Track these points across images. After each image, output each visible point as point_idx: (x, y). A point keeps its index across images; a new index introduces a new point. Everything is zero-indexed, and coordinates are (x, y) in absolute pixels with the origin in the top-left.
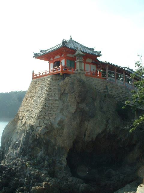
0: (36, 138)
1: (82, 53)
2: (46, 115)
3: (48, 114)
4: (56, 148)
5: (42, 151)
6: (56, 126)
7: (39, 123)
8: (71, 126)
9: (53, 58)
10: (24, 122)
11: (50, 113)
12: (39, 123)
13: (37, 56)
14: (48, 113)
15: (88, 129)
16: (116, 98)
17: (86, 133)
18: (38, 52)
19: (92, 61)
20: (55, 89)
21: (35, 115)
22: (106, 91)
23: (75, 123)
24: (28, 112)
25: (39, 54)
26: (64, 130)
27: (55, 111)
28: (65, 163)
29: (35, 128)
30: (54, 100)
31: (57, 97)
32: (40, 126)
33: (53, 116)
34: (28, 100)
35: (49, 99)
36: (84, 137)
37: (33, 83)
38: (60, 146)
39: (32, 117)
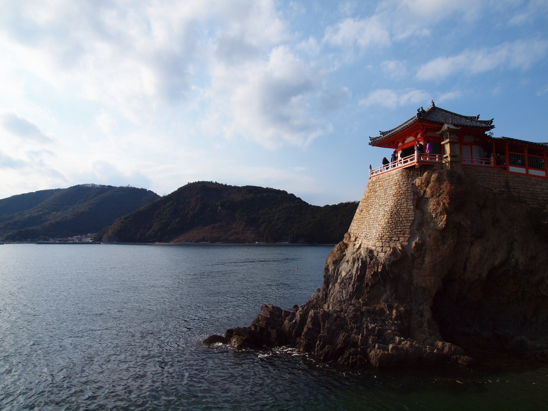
5: (388, 292)
7: (382, 247)
9: (403, 142)
10: (357, 246)
13: (376, 142)
16: (528, 203)
18: (376, 134)
20: (407, 192)
21: (375, 234)
24: (364, 230)
25: (378, 138)
26: (425, 259)
27: (408, 227)
28: (428, 315)
31: (411, 204)
33: (406, 235)
34: (363, 212)
35: (398, 208)
37: (371, 185)
38: (419, 286)
39: (371, 237)
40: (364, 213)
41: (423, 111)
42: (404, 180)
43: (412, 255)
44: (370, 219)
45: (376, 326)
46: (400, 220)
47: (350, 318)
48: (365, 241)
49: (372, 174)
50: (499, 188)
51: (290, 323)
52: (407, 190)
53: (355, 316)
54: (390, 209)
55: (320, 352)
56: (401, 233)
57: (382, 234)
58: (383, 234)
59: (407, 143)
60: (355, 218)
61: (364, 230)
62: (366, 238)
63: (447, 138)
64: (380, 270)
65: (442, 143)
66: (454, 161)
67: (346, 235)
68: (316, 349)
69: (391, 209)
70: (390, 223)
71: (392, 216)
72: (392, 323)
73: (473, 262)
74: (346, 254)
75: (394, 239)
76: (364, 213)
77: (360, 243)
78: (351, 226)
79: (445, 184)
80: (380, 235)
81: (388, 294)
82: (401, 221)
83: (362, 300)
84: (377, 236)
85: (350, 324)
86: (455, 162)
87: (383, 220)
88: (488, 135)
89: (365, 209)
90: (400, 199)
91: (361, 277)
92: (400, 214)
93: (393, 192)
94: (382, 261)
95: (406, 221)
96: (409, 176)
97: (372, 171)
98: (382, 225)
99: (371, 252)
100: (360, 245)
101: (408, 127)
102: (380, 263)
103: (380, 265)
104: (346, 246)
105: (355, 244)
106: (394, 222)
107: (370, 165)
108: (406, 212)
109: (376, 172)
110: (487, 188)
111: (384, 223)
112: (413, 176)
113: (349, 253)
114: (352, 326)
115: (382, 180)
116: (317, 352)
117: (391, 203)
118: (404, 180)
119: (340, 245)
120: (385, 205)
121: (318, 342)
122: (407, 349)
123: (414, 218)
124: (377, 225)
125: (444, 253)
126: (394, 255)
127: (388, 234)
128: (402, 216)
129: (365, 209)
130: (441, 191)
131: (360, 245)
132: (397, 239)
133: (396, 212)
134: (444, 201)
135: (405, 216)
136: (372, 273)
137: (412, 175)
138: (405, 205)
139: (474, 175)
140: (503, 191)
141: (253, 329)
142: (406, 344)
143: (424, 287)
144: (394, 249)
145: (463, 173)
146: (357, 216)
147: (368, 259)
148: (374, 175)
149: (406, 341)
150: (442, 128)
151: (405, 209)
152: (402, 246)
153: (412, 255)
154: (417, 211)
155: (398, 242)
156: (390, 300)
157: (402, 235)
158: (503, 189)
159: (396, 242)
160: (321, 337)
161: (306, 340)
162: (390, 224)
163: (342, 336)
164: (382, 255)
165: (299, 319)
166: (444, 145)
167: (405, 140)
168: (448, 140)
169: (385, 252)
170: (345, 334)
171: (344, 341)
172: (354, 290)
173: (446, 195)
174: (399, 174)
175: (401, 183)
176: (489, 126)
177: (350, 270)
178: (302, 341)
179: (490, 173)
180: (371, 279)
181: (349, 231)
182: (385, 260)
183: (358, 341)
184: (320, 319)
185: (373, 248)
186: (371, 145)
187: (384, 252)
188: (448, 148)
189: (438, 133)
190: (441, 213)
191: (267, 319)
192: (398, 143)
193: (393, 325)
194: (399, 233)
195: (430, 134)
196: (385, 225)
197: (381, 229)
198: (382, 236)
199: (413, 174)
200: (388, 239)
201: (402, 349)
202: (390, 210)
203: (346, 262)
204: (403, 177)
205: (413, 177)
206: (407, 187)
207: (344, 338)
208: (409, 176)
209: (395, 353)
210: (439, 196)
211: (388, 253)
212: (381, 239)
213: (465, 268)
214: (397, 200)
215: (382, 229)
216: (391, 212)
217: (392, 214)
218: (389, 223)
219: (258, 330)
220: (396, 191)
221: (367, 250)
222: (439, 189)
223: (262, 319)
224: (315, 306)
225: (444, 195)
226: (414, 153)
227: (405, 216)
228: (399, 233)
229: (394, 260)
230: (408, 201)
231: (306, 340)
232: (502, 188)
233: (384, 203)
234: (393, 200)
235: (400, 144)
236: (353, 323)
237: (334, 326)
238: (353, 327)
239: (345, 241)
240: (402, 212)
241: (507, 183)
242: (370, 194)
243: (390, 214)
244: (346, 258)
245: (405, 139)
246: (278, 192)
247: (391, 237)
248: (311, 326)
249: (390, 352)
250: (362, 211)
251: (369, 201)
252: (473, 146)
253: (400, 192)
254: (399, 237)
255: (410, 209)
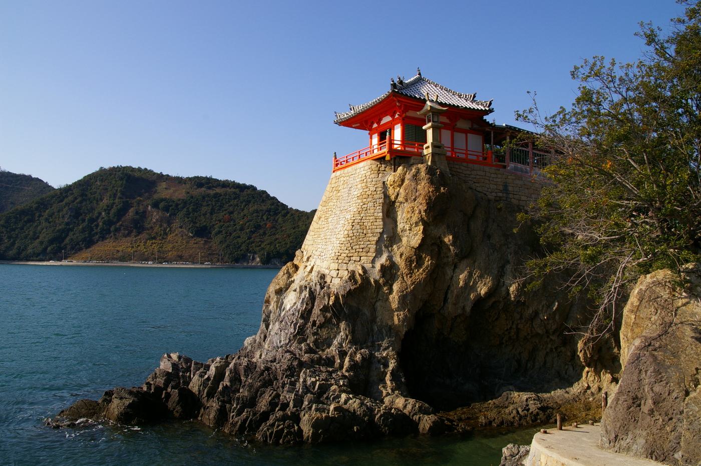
0: (328, 303)
1: (440, 108)
2: (354, 251)
3: (357, 250)
4: (376, 328)
6: (375, 274)
7: (338, 270)
8: (410, 277)
9: (378, 123)
10: (309, 268)
11: (363, 246)
12: (338, 270)
13: (348, 123)
14: (357, 247)
15: (453, 285)
17: (449, 296)
19: (472, 125)
20: (375, 192)
21: (331, 252)
22: (505, 195)
23: (420, 274)
24: (319, 246)
29: (328, 279)
30: (374, 217)
31: (380, 211)
32: (339, 276)
33: (369, 254)
34: (321, 219)
35: (362, 215)
36: (444, 304)
39: (326, 256)
40: (322, 221)
41: (401, 82)
42: (373, 176)
43: (376, 281)
44: (328, 230)
45: (316, 381)
46: (363, 233)
47: (283, 370)
48: (318, 262)
49: (337, 165)
50: (496, 193)
51: (200, 380)
52: (375, 190)
53: (290, 368)
54: (352, 216)
55: (236, 419)
56: (364, 250)
57: (339, 252)
58: (341, 251)
59: (384, 124)
60: (311, 228)
61: (319, 246)
62: (320, 257)
63: (429, 121)
64: (331, 303)
65: (424, 128)
66: (436, 154)
67: (298, 253)
68: (232, 414)
69: (354, 217)
70: (350, 236)
71: (353, 226)
72: (342, 376)
73: (455, 291)
74: (294, 280)
75: (354, 258)
76: (322, 221)
77: (312, 265)
78: (305, 240)
79: (423, 184)
80: (337, 254)
81: (342, 336)
82: (365, 234)
83: (304, 345)
84: (333, 255)
85: (282, 378)
86: (439, 154)
87: (342, 232)
88: (490, 123)
89: (324, 216)
90: (366, 203)
91: (306, 315)
92: (364, 224)
93: (356, 192)
94: (334, 289)
95: (372, 234)
96: (379, 170)
97: (337, 161)
98: (340, 240)
99: (323, 277)
100: (312, 268)
101: (380, 103)
102: (332, 293)
103: (331, 295)
104: (296, 268)
105: (306, 266)
106: (355, 234)
107: (335, 153)
108: (371, 221)
109: (341, 162)
110: (481, 192)
111: (342, 236)
112: (385, 171)
113: (299, 278)
114: (284, 382)
115: (347, 174)
116: (232, 418)
117: (354, 209)
118: (373, 176)
119: (287, 267)
120: (347, 210)
121: (235, 405)
122: (354, 410)
123: (382, 230)
124: (335, 239)
125: (417, 279)
126: (351, 281)
127: (347, 251)
128: (366, 226)
129: (324, 216)
130: (417, 194)
131: (312, 268)
132: (359, 260)
133: (360, 221)
134: (420, 207)
135: (370, 227)
136: (322, 307)
137: (384, 169)
138: (372, 211)
139: (465, 174)
140: (500, 197)
141: (146, 390)
142: (354, 404)
143: (390, 326)
144: (353, 273)
145: (448, 171)
146: (314, 226)
147: (318, 287)
148: (339, 166)
149: (354, 400)
150: (424, 106)
151: (371, 218)
152: (363, 268)
153: (376, 281)
154: (387, 220)
155: (359, 263)
156: (344, 345)
157: (364, 254)
158: (500, 194)
159: (356, 263)
160: (238, 399)
161: (218, 403)
162: (350, 238)
163: (269, 395)
164: (337, 281)
165: (214, 374)
166: (425, 131)
167: (380, 120)
168: (430, 124)
169: (341, 278)
170: (273, 392)
171: (270, 402)
172: (295, 332)
173: (422, 200)
174: (367, 168)
175: (369, 180)
176: (487, 109)
177: (295, 303)
178: (214, 405)
179: (486, 172)
180: (320, 316)
181: (303, 247)
182: (339, 289)
183: (290, 401)
184: (242, 372)
185: (326, 272)
186: (336, 123)
187: (340, 278)
188: (430, 134)
189: (418, 113)
190: (417, 224)
191: (168, 373)
192: (373, 124)
193: (342, 379)
194: (361, 250)
195: (411, 114)
196: (344, 239)
197: (339, 245)
198: (339, 254)
199: (385, 167)
200: (346, 258)
201: (347, 410)
202: (352, 218)
203: (293, 291)
204: (372, 172)
205: (385, 172)
206: (375, 186)
207: (270, 398)
208: (379, 170)
209: (336, 416)
210: (415, 200)
211: (344, 278)
212: (337, 259)
213: (445, 300)
214: (362, 204)
215: (339, 245)
216: (352, 221)
217: (354, 224)
218: (349, 237)
219: (151, 390)
220: (361, 191)
221: (319, 274)
222: (415, 191)
223: (160, 375)
224: (248, 355)
225: (420, 200)
226: (386, 139)
227: (370, 227)
228: (361, 250)
229: (350, 289)
230: (376, 205)
231: (218, 403)
232: (500, 193)
233: (346, 208)
234: (357, 204)
235: (375, 125)
236: (285, 378)
237: (259, 382)
238: (286, 382)
239: (296, 262)
240: (367, 221)
241: (506, 186)
242: (332, 194)
243: (351, 224)
244: (294, 286)
245: (380, 118)
246: (243, 188)
247: (350, 257)
248: (228, 384)
249: (330, 414)
250: (320, 218)
251: (329, 204)
252: (468, 134)
253: (367, 193)
254: (360, 257)
255: (377, 217)
